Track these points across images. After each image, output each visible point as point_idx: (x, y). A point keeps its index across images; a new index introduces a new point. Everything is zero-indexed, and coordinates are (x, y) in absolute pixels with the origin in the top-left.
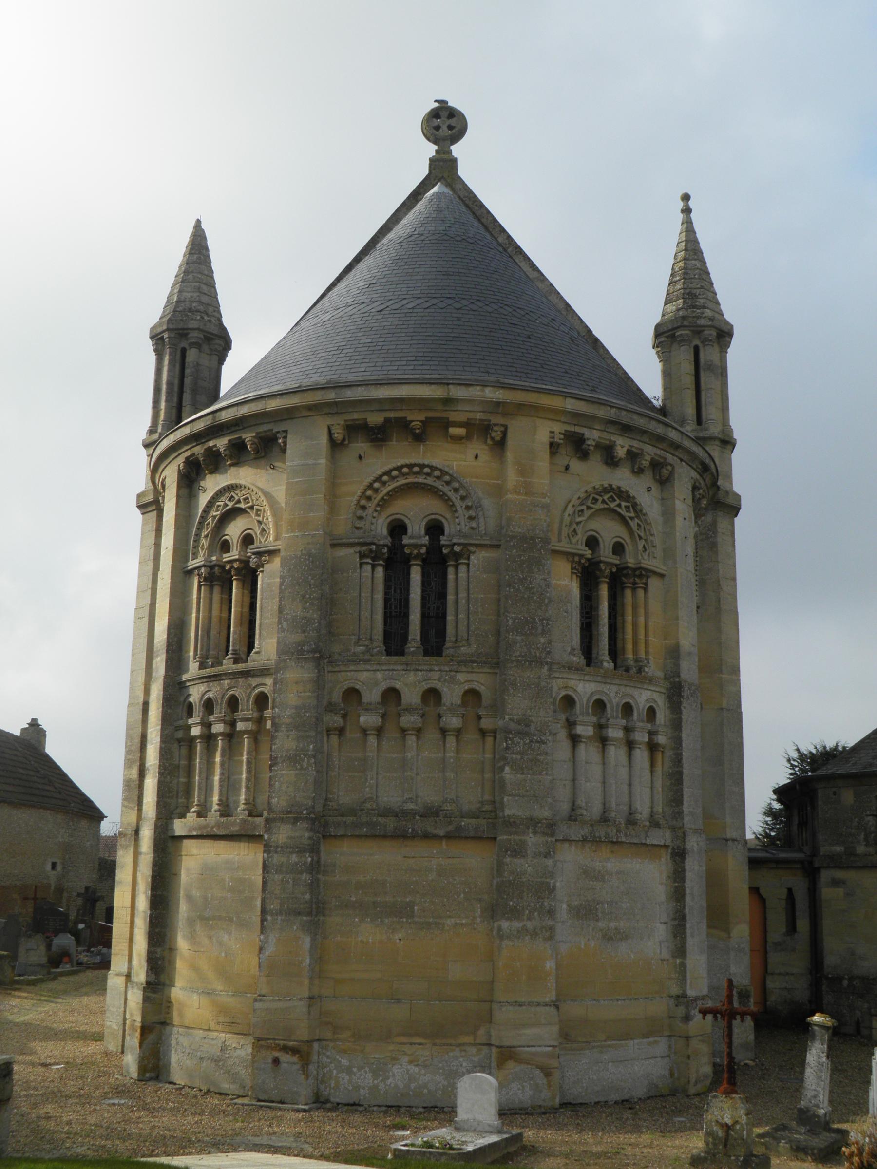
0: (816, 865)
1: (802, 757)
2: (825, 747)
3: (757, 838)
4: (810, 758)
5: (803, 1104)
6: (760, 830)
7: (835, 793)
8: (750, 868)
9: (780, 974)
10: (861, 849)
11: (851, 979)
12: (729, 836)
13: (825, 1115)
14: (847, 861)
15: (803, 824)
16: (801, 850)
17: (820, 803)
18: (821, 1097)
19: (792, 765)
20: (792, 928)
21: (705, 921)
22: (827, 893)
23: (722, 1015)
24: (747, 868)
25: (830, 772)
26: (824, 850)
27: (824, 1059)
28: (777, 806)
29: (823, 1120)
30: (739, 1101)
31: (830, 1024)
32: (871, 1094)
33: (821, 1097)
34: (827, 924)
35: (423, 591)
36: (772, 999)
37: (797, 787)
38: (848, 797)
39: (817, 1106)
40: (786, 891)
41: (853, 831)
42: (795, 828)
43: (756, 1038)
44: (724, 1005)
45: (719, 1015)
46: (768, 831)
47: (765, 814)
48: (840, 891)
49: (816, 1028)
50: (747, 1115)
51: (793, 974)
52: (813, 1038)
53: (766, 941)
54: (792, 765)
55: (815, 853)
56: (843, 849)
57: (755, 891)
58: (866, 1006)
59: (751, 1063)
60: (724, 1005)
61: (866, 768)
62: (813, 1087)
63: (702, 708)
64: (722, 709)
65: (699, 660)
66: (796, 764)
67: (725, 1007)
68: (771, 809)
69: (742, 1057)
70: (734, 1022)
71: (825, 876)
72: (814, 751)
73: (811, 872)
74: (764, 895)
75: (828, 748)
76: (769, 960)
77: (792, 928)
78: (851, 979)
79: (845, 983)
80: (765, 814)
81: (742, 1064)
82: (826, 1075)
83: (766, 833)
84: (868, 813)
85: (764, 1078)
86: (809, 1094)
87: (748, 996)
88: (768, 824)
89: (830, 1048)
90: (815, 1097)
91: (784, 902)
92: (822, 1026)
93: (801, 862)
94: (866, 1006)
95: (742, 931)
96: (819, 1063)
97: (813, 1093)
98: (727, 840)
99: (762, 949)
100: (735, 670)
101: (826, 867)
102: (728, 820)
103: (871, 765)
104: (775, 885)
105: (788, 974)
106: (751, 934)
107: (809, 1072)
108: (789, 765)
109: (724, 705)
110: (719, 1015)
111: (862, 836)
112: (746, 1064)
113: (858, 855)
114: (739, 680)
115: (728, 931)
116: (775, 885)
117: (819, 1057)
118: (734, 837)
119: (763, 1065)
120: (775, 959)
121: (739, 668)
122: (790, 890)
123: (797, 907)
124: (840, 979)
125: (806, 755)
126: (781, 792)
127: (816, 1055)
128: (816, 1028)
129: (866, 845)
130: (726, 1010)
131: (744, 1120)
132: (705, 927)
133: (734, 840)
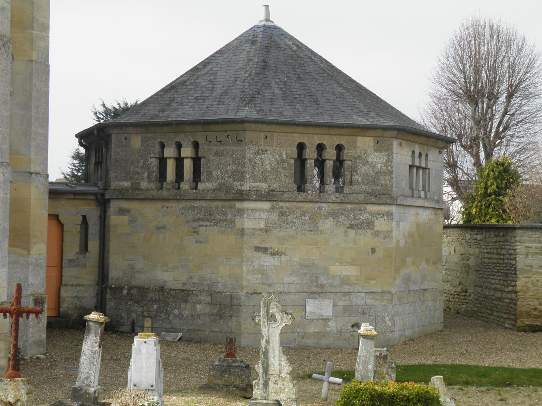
0: (107, 197)
1: (107, 111)
2: (126, 104)
3: (66, 177)
4: (114, 112)
5: (77, 384)
6: (68, 171)
7: (126, 138)
8: (50, 198)
9: (72, 285)
10: (144, 185)
11: (130, 288)
12: (33, 170)
13: (95, 392)
14: (132, 195)
15: (98, 163)
16: (95, 185)
17: (113, 146)
18: (93, 378)
19: (98, 118)
20: (84, 248)
21: (7, 240)
22: (114, 219)
23: (10, 314)
24: (47, 197)
25: (123, 121)
26: (114, 184)
27: (97, 348)
28: (82, 151)
29: (92, 396)
30: (21, 383)
31: (103, 320)
32: (130, 372)
33: (93, 378)
34: (113, 245)
35: (414, 366)
36: (64, 306)
37: (95, 132)
38: (136, 141)
39: (89, 385)
40: (81, 218)
41: (139, 170)
42: (92, 166)
43: (48, 337)
44: (12, 305)
45: (8, 314)
46: (74, 172)
47: (73, 157)
48: (125, 219)
49: (91, 323)
50: (27, 394)
51: (83, 285)
52: (89, 332)
53: (62, 259)
54: (98, 118)
55: (106, 187)
56: (129, 184)
57: (54, 217)
58: (140, 309)
59: (42, 357)
60: (12, 305)
61: (152, 119)
62: (86, 371)
63: (13, 59)
64: (32, 61)
65: (12, 16)
66: (102, 117)
67: (13, 307)
68: (78, 153)
69: (31, 351)
70: (21, 319)
71: (114, 206)
72: (117, 107)
73: (103, 203)
74: (63, 222)
75: (129, 105)
76: (64, 274)
77: (84, 248)
78: (130, 288)
79: (125, 292)
80: (73, 157)
81: (35, 357)
82: (98, 362)
83: (73, 173)
84: (152, 156)
85: (51, 368)
86: (82, 376)
87: (43, 303)
88: (75, 166)
89: (102, 339)
90: (87, 378)
91: (78, 227)
92: (96, 322)
93: (95, 194)
94: (140, 309)
95: (40, 250)
96: (92, 352)
97: (86, 376)
98: (31, 173)
99: (58, 265)
100: (46, 28)
101: (116, 199)
102: (33, 156)
103: (157, 116)
104: (71, 212)
105: (79, 285)
106: (48, 252)
107: (84, 359)
108: (95, 118)
109: (34, 57)
110: (8, 314)
111: (146, 174)
112: (38, 358)
113: (142, 190)
114: (48, 37)
115: (28, 249)
116: (71, 212)
117: (93, 347)
118: (37, 171)
119: (52, 358)
120: (68, 272)
121: (49, 26)
122: (84, 217)
123: (90, 231)
124: (121, 289)
125: (110, 110)
126: (84, 137)
127: (90, 345)
128: (91, 323)
129: (148, 182)
130: (14, 310)
131: (25, 398)
132: (7, 245)
133: (37, 174)
